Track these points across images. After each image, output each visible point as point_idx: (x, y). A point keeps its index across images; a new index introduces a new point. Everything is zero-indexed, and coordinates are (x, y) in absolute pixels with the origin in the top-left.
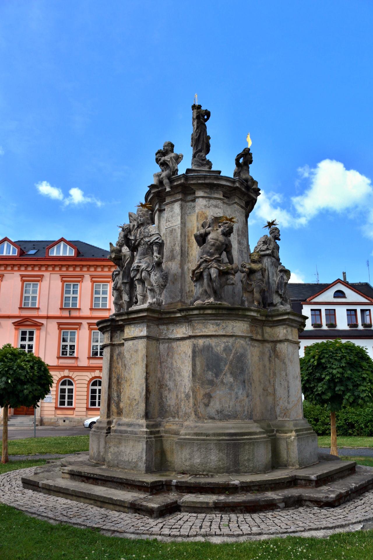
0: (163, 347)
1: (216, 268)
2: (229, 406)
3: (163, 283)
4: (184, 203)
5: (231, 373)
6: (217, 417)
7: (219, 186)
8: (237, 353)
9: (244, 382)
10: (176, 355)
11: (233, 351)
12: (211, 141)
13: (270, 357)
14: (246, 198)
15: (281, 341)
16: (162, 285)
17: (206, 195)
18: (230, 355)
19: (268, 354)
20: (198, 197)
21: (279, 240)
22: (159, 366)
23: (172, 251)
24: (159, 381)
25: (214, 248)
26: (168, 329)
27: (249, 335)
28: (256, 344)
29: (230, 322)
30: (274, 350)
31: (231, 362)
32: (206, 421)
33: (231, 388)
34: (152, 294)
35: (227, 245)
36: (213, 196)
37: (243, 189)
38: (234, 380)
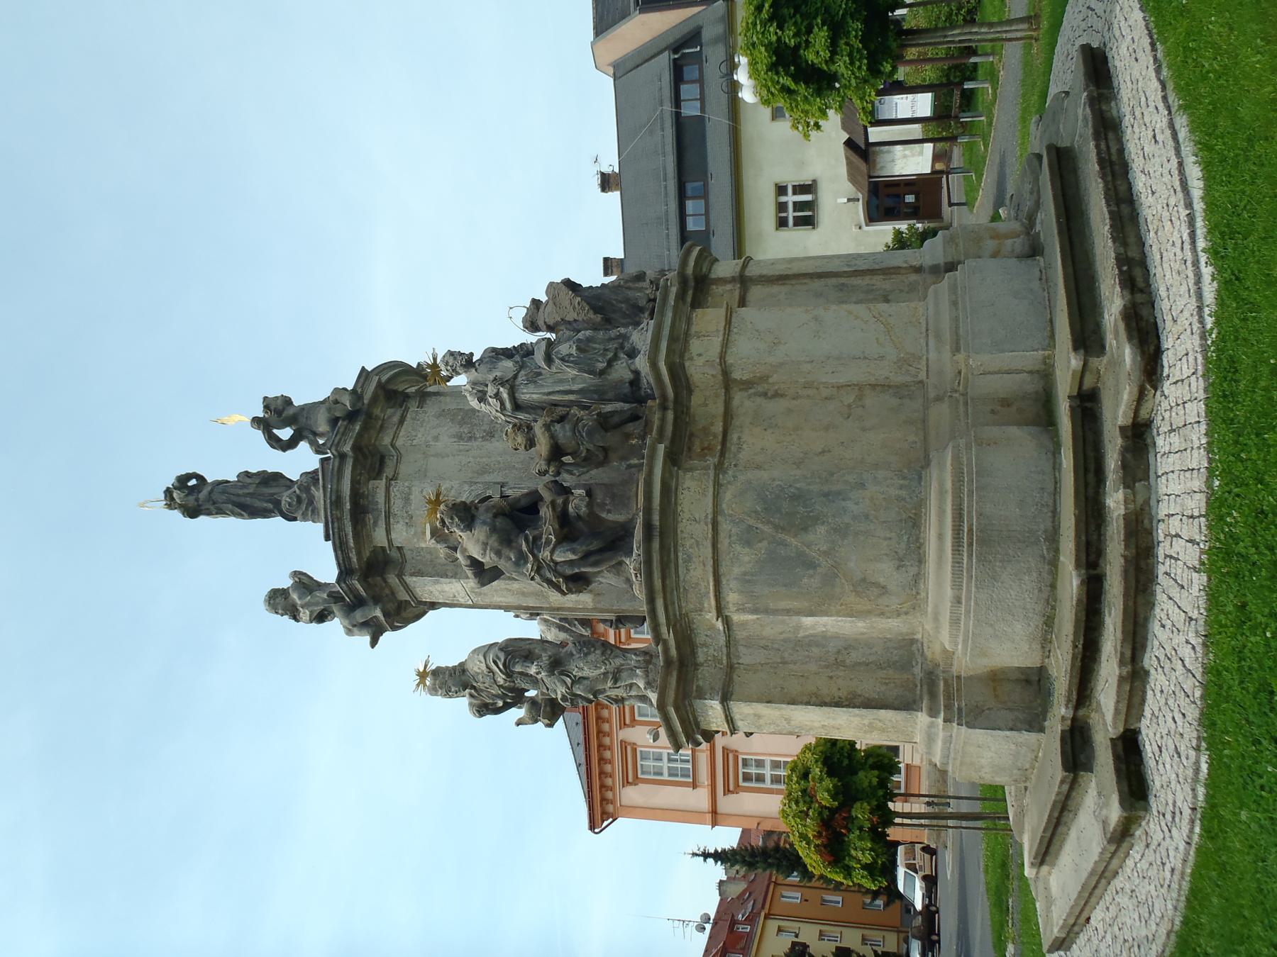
0: (746, 657)
1: (552, 552)
2: (885, 539)
3: (598, 652)
4: (408, 568)
5: (805, 529)
6: (913, 571)
7: (356, 495)
8: (756, 512)
9: (826, 495)
10: (764, 633)
11: (751, 522)
12: (253, 470)
13: (765, 395)
14: (377, 411)
15: (726, 373)
16: (603, 654)
17: (382, 523)
18: (762, 532)
19: (759, 400)
20: (390, 541)
21: (472, 354)
22: (791, 666)
23: (523, 594)
24: (827, 667)
25: (506, 551)
26: (705, 645)
27: (712, 473)
28: (735, 437)
29: (681, 527)
30: (747, 385)
31: (777, 528)
32: (923, 595)
33: (841, 531)
34: (624, 675)
35: (495, 516)
36: (382, 506)
37: (358, 428)
38: (823, 524)
